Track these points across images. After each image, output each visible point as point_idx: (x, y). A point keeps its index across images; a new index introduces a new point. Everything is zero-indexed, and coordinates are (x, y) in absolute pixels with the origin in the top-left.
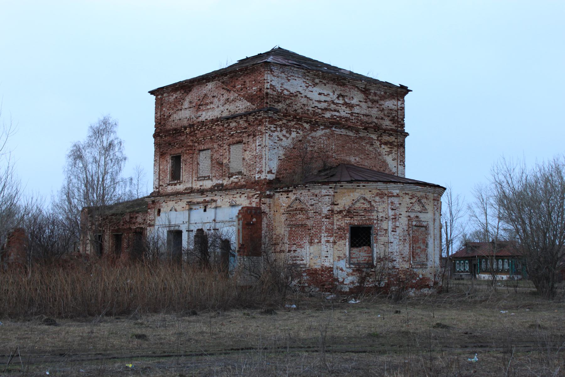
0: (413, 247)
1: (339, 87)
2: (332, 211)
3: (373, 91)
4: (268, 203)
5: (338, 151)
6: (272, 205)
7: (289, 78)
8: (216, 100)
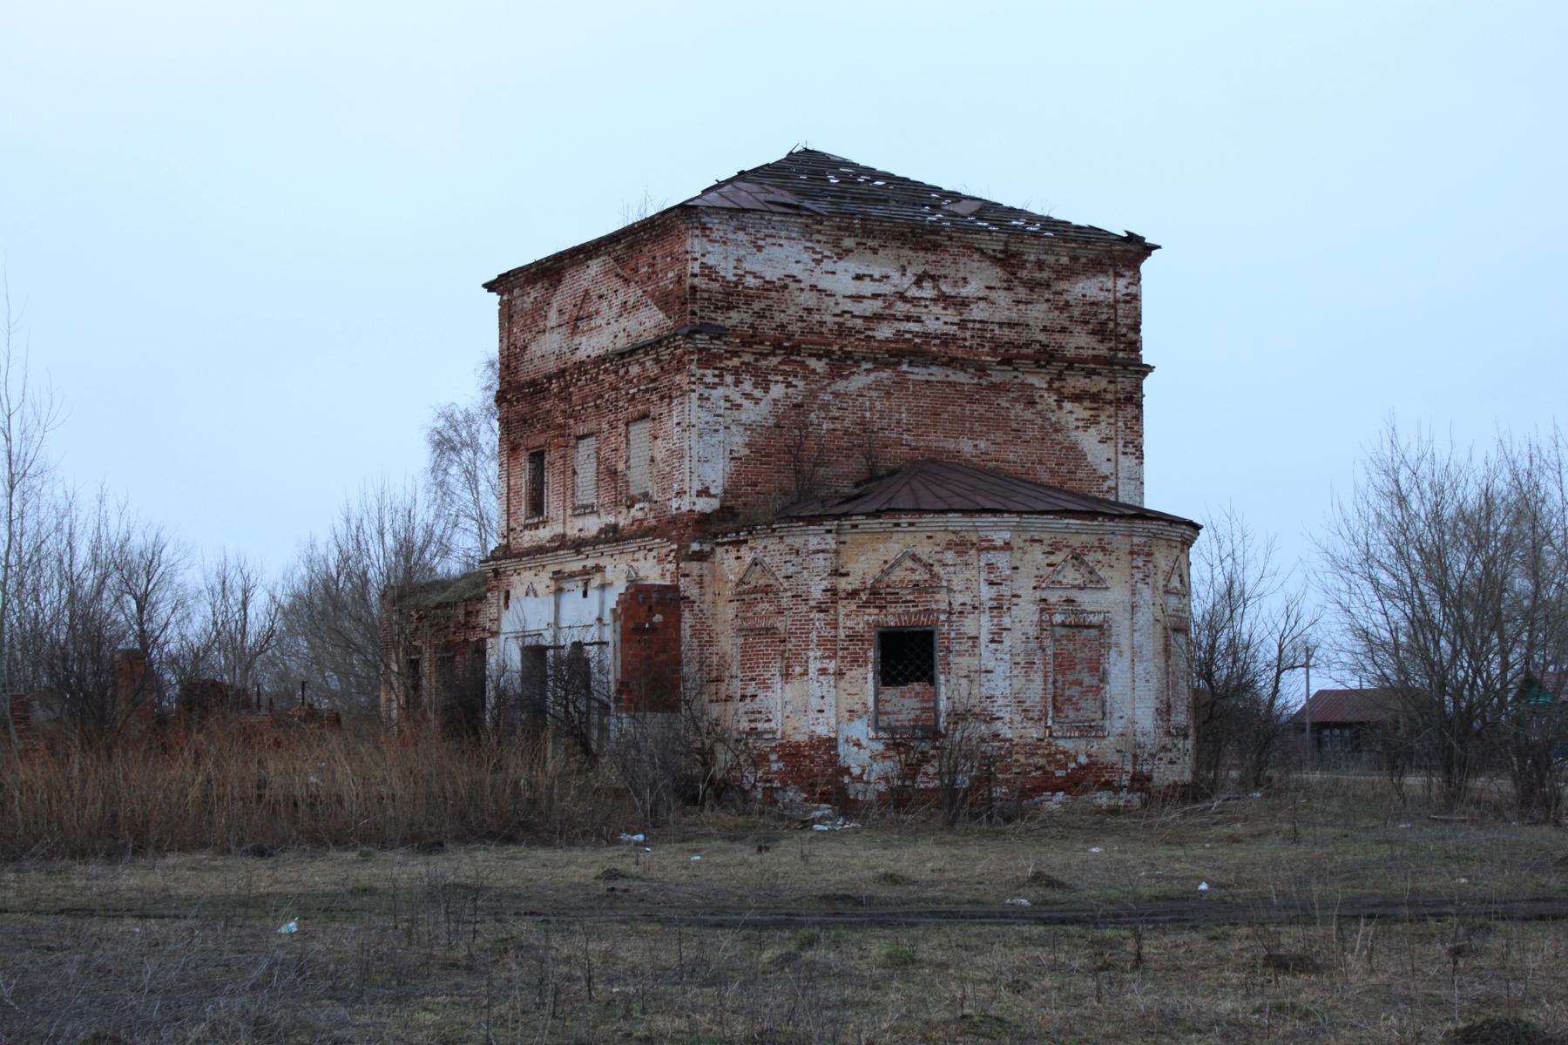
0: (1055, 681)
1: (921, 254)
2: (833, 591)
3: (1032, 258)
4: (696, 572)
5: (917, 426)
6: (707, 579)
7: (760, 243)
8: (605, 304)
